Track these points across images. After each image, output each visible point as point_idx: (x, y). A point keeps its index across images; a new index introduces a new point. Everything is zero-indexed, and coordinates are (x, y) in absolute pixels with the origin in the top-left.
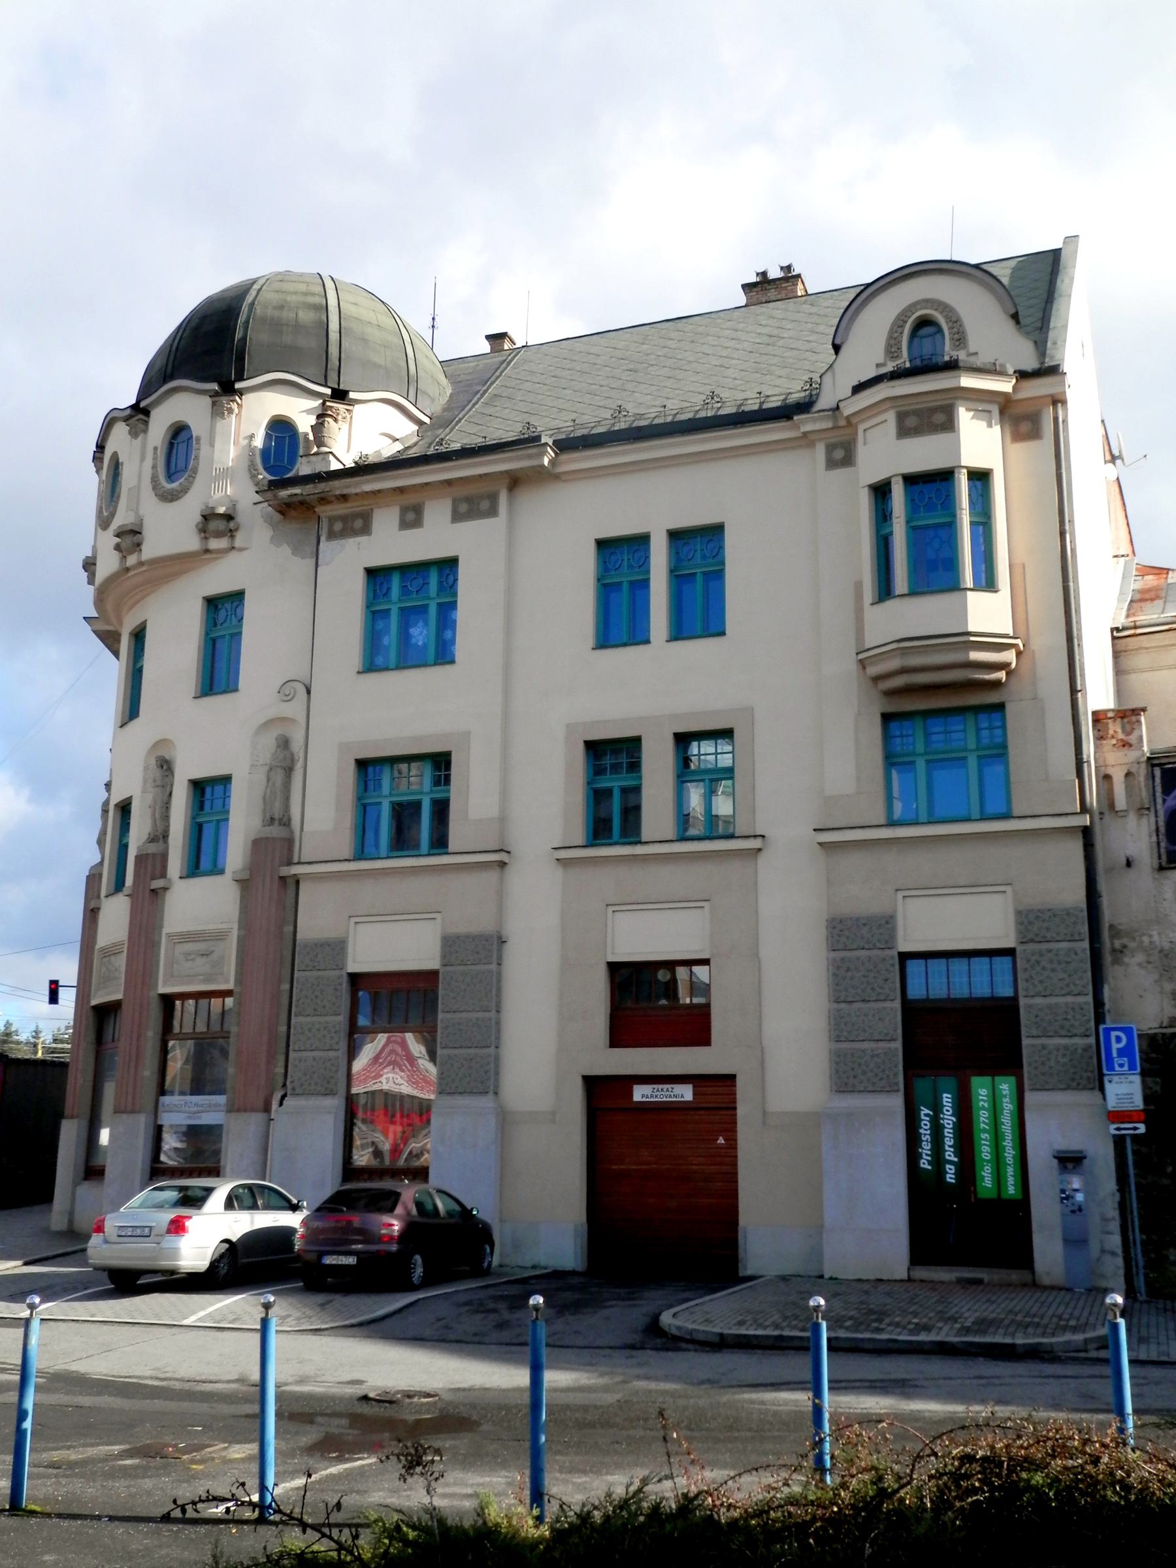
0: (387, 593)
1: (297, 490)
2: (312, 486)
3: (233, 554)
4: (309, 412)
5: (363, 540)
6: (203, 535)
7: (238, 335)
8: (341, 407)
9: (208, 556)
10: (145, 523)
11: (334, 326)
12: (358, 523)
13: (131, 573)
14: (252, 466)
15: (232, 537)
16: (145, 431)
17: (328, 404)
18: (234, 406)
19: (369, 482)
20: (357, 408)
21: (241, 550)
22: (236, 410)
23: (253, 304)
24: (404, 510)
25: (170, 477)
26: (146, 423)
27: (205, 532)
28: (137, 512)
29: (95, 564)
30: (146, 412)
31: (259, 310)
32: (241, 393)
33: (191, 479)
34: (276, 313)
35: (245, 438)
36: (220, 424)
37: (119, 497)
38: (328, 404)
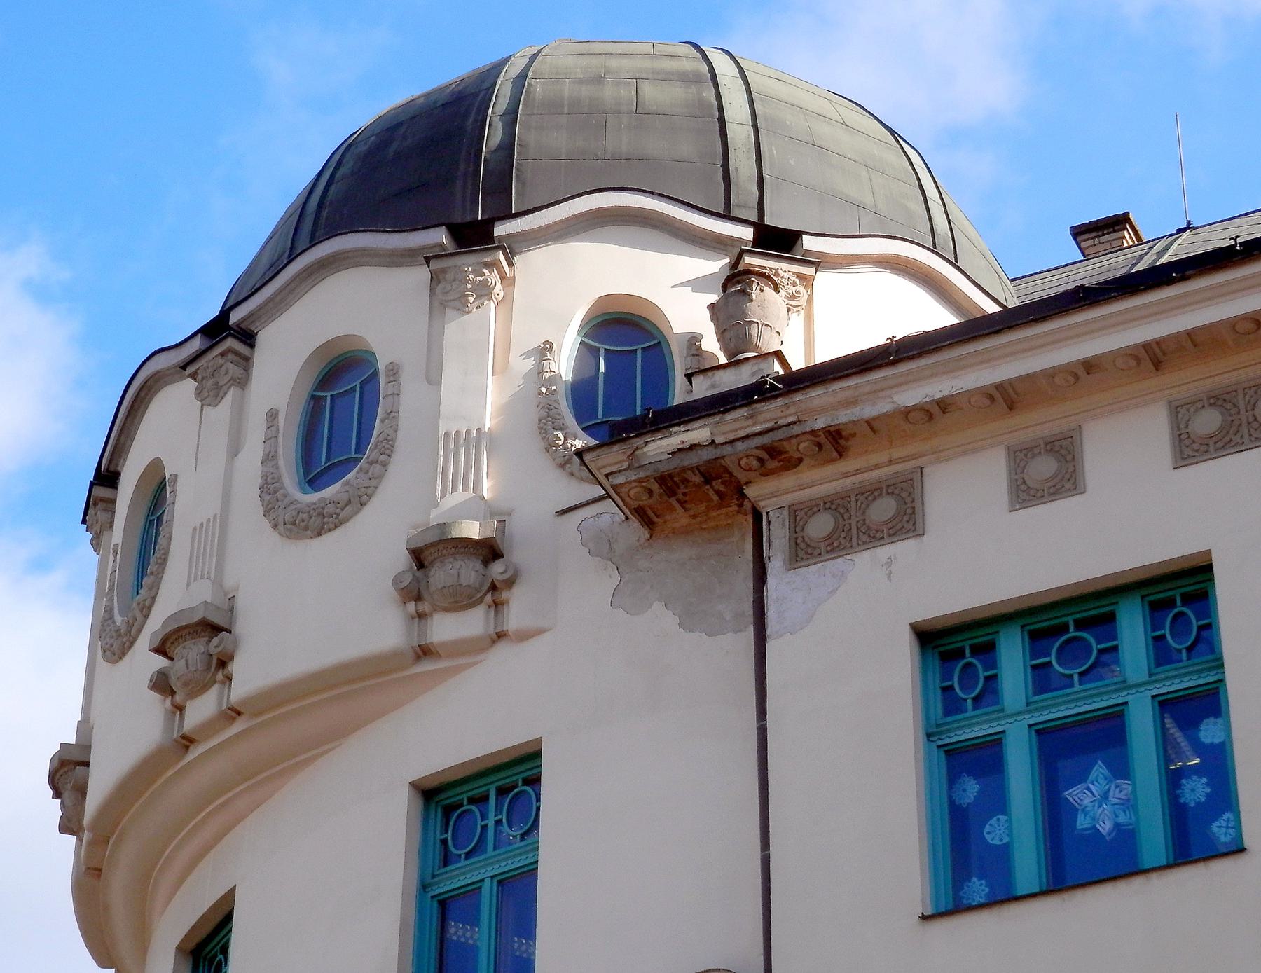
0: (989, 692)
1: (698, 433)
2: (743, 412)
3: (503, 651)
4: (698, 285)
5: (903, 550)
6: (411, 607)
7: (493, 137)
8: (783, 269)
9: (426, 666)
10: (240, 604)
11: (736, 110)
12: (883, 509)
13: (196, 751)
14: (548, 421)
15: (497, 605)
16: (243, 382)
17: (749, 260)
18: (492, 277)
19: (918, 378)
20: (824, 280)
21: (525, 636)
22: (499, 289)
23: (523, 76)
24: (1020, 457)
25: (313, 481)
26: (246, 361)
27: (418, 598)
28: (218, 583)
29: (86, 764)
30: (248, 337)
31: (538, 88)
32: (511, 248)
33: (377, 468)
34: (586, 91)
35: (527, 355)
36: (455, 329)
37: (163, 562)
38: (749, 260)
